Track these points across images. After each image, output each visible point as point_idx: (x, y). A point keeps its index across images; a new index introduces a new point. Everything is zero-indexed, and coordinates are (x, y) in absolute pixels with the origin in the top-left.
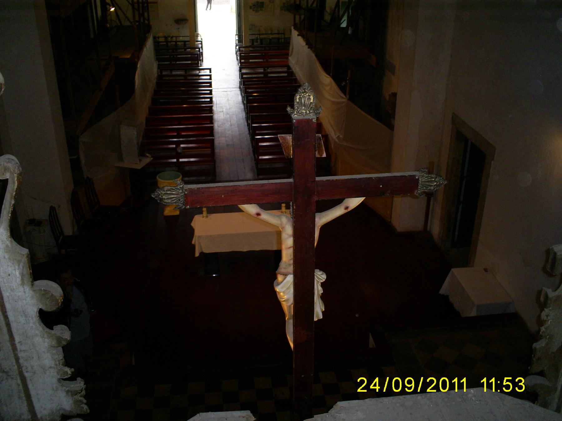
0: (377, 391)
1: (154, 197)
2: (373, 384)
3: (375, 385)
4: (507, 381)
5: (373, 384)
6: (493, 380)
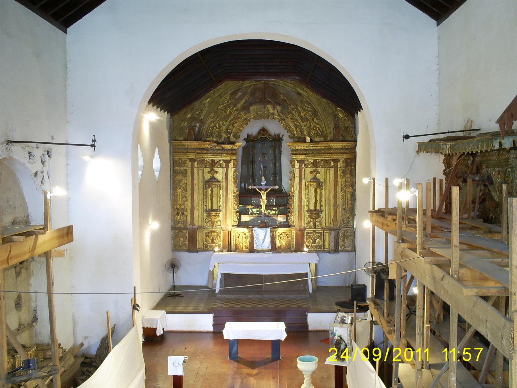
2: (343, 354)
4: (467, 351)
5: (343, 354)
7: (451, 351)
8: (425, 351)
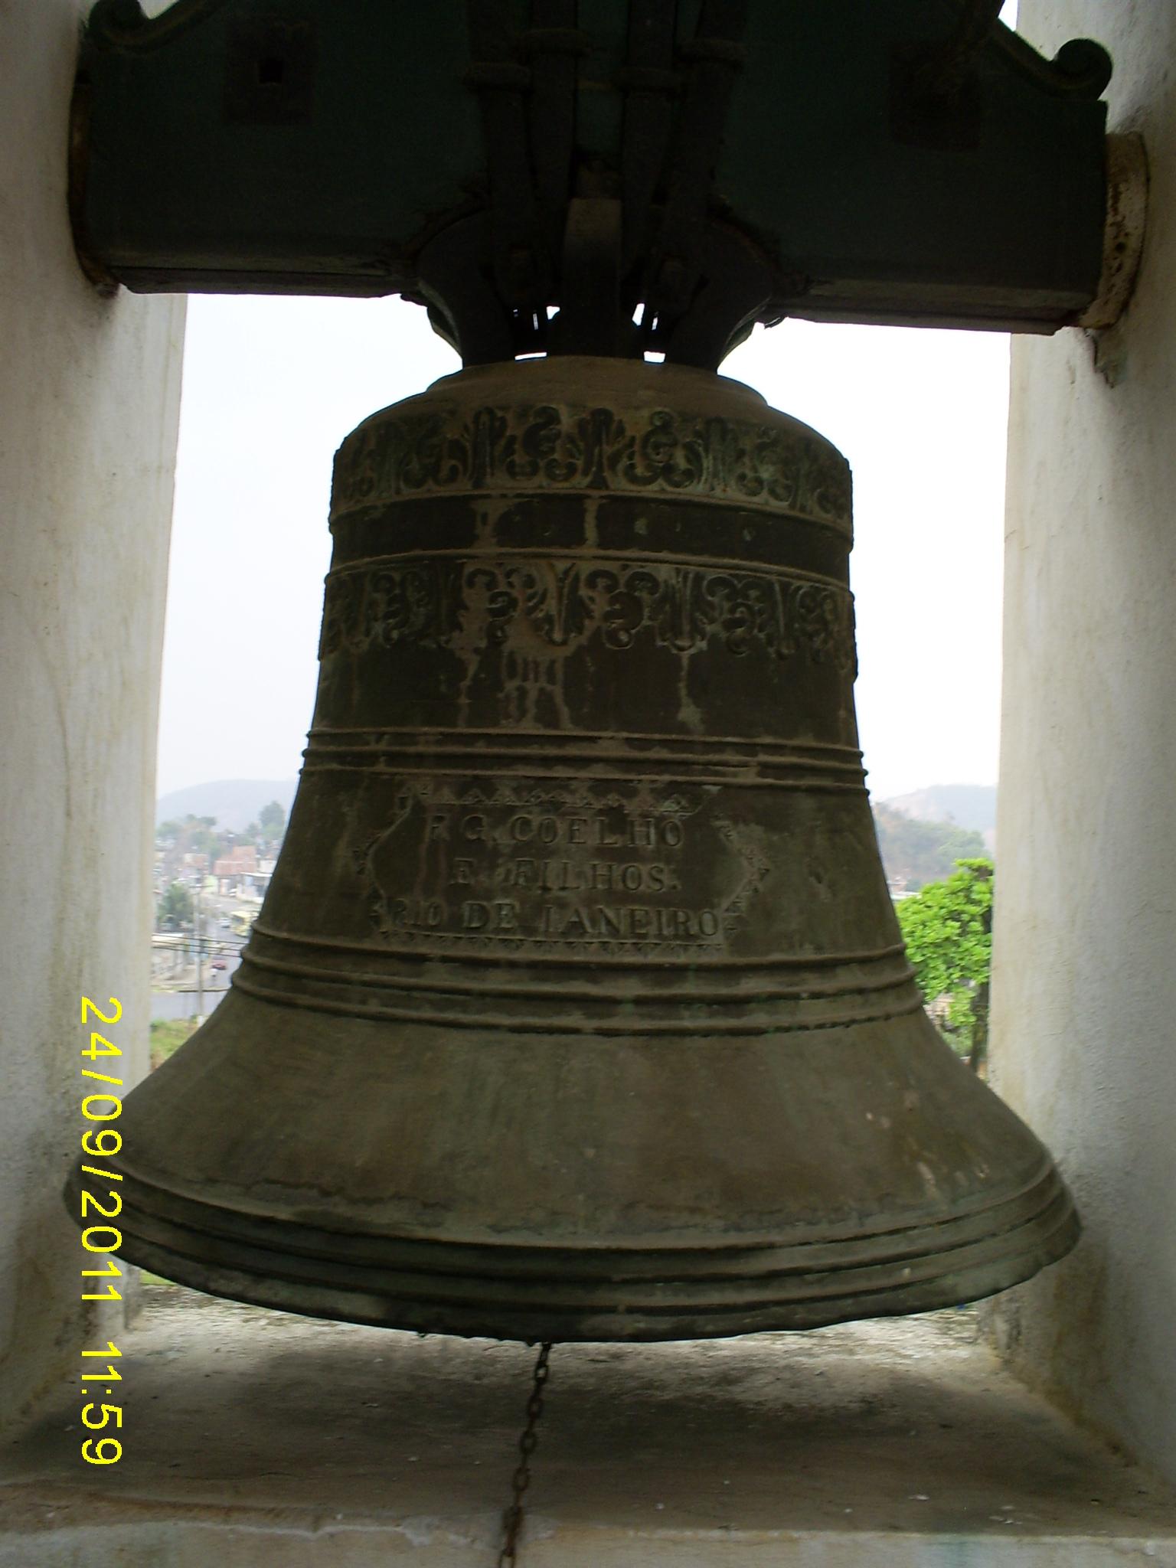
0: (84, 1053)
1: (662, 506)
2: (103, 1040)
3: (99, 1046)
4: (113, 1415)
5: (103, 1040)
6: (115, 1376)
7: (111, 1264)
8: (111, 1368)
